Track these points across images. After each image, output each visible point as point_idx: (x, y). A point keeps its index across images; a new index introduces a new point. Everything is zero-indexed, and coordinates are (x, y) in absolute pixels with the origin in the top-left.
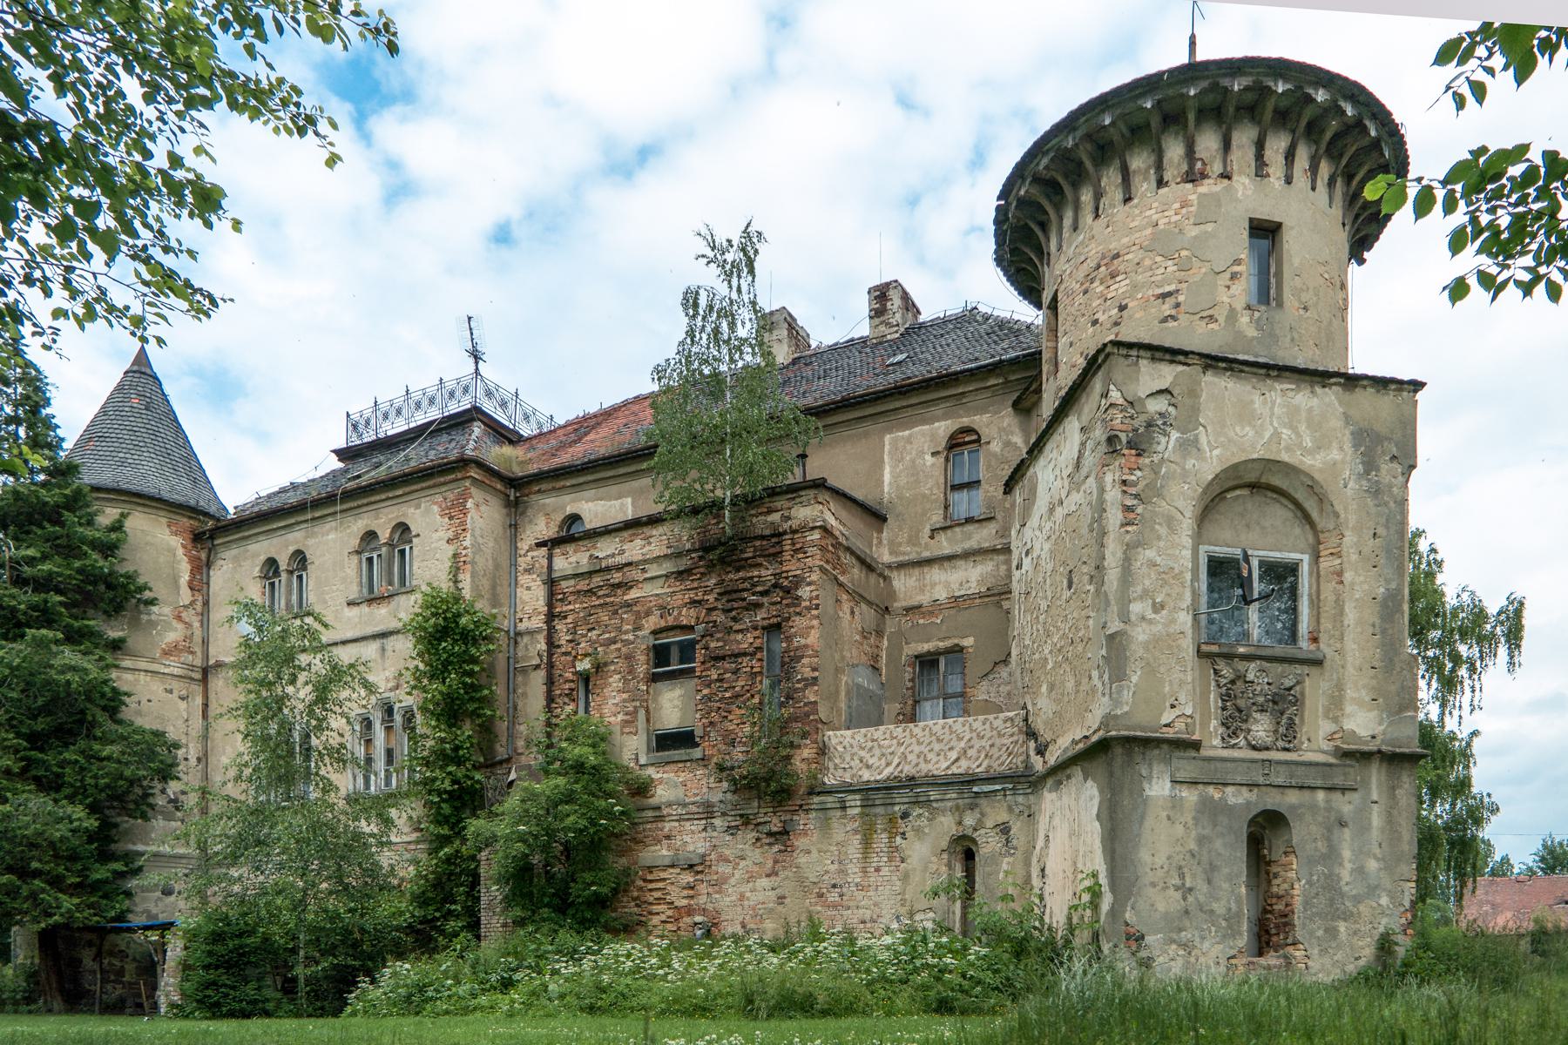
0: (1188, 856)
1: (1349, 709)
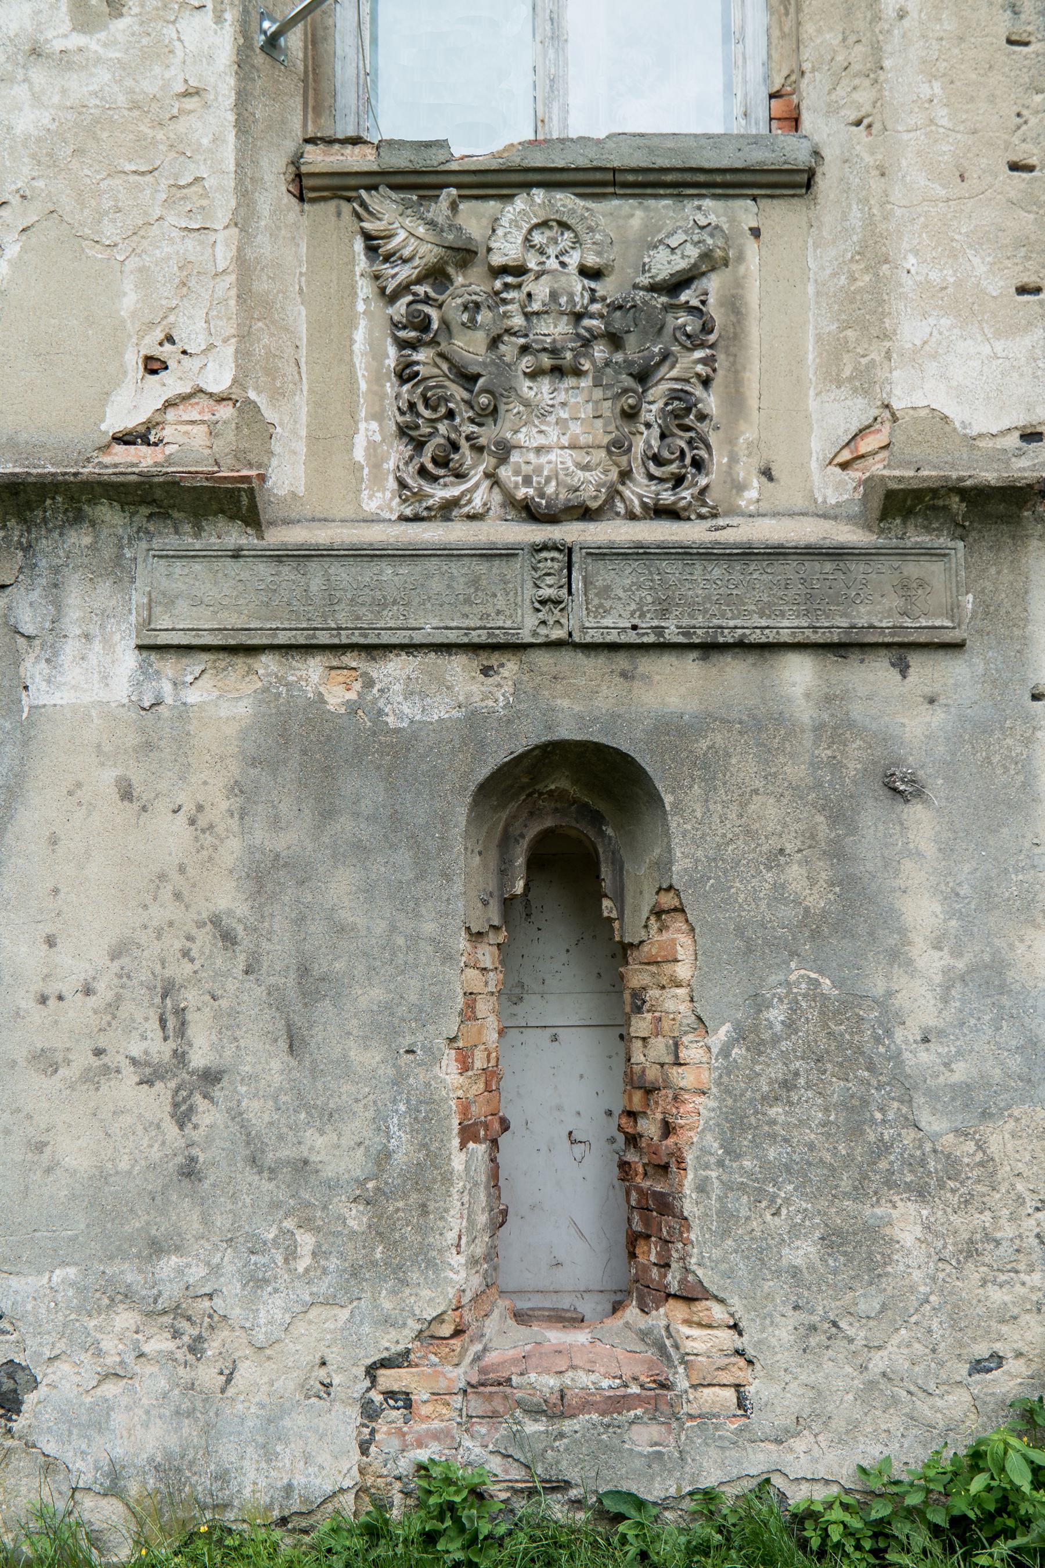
0: (205, 937)
1: (912, 330)
